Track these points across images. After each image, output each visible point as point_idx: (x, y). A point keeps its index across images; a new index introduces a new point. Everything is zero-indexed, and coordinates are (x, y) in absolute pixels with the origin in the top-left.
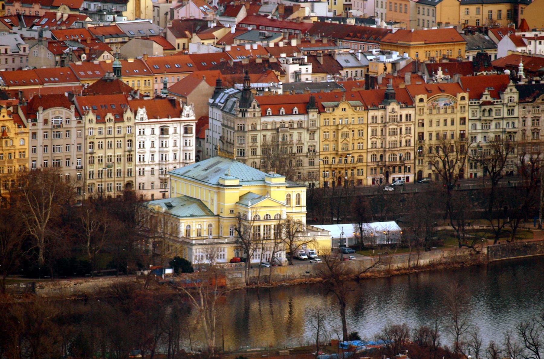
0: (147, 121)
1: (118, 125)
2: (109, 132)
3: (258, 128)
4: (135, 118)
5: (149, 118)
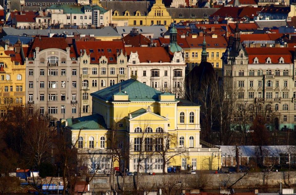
0: (139, 64)
1: (111, 66)
2: (104, 72)
3: (246, 74)
4: (128, 61)
5: (141, 62)
